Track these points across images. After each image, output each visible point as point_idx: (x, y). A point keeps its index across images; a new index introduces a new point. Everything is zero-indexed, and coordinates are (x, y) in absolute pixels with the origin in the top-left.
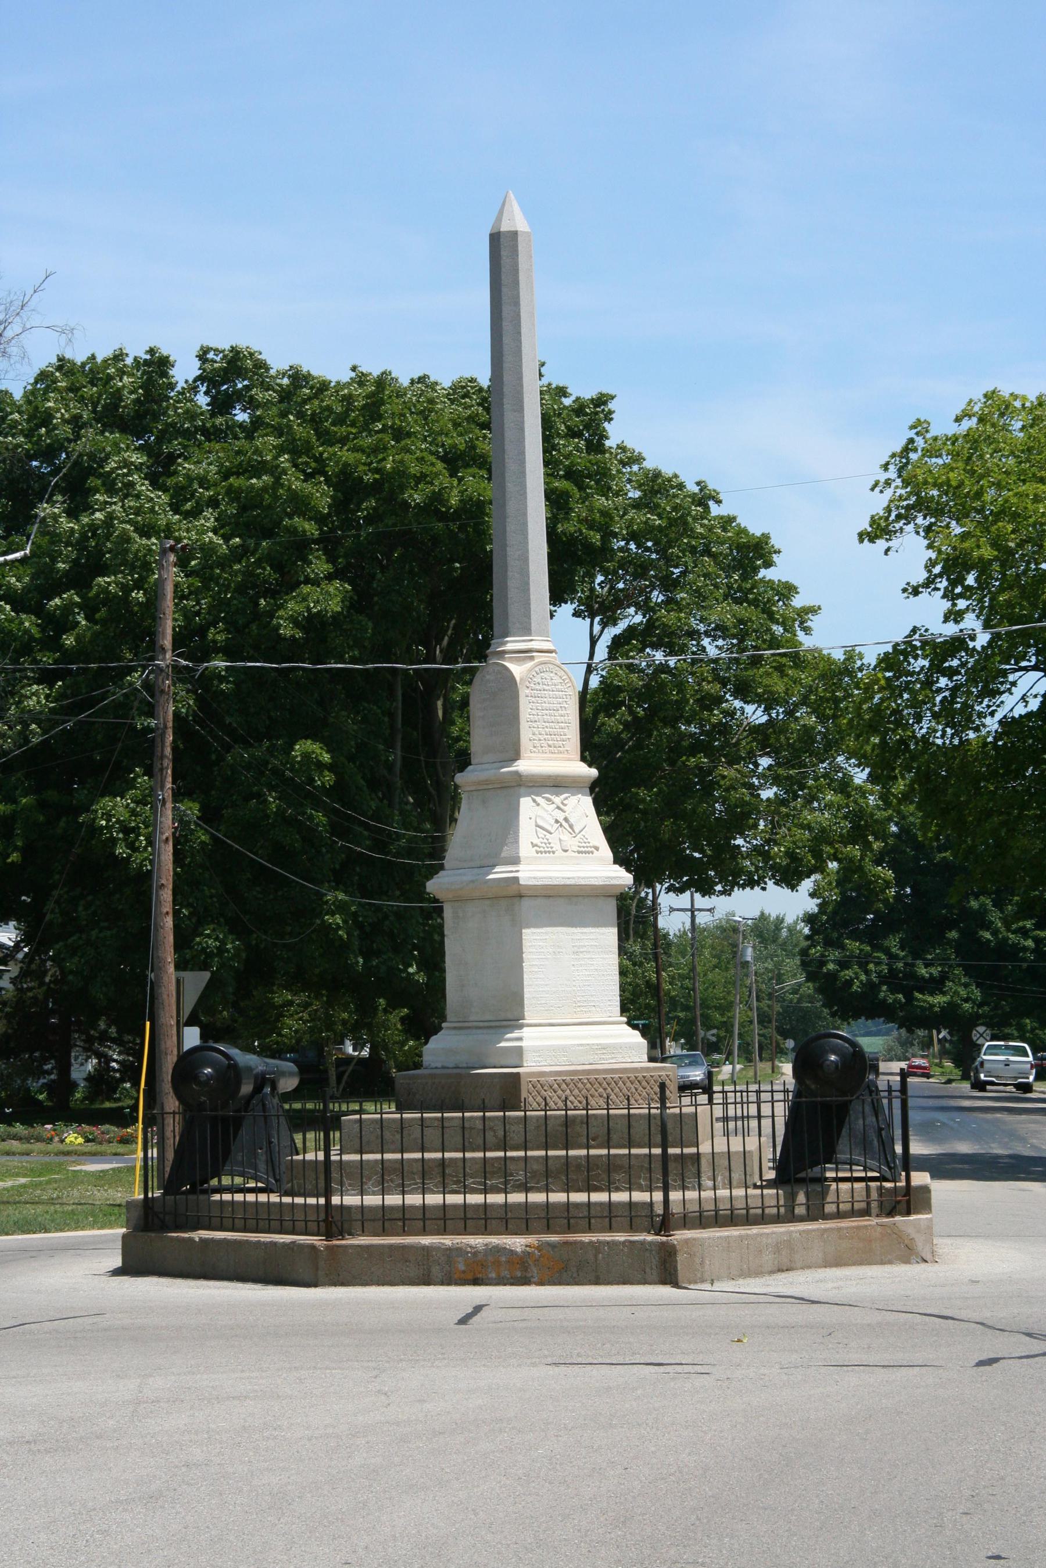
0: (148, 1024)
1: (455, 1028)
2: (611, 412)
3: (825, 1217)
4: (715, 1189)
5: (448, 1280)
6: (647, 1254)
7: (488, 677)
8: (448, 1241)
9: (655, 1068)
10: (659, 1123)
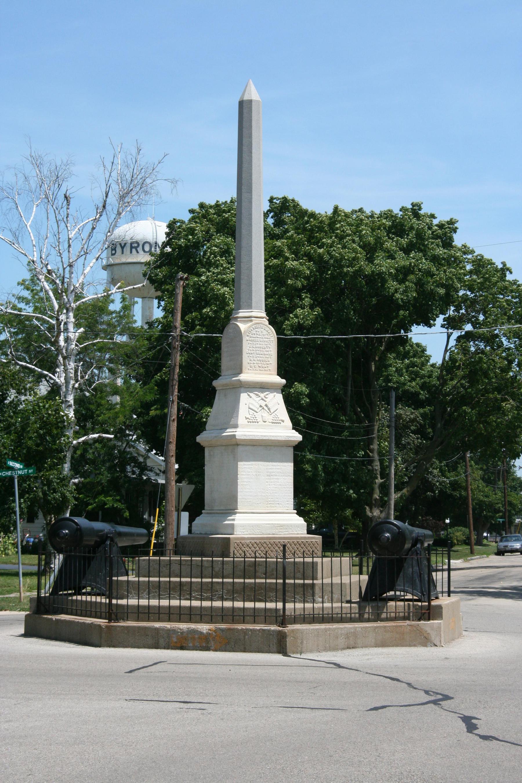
0: (158, 509)
1: (208, 513)
2: (457, 228)
3: (382, 620)
4: (323, 603)
5: (168, 647)
6: (271, 637)
7: (230, 330)
8: (168, 625)
9: (309, 538)
10: (282, 566)
